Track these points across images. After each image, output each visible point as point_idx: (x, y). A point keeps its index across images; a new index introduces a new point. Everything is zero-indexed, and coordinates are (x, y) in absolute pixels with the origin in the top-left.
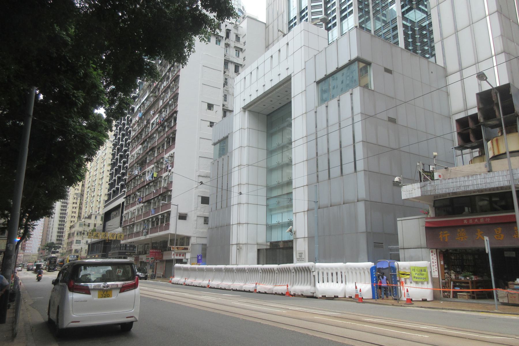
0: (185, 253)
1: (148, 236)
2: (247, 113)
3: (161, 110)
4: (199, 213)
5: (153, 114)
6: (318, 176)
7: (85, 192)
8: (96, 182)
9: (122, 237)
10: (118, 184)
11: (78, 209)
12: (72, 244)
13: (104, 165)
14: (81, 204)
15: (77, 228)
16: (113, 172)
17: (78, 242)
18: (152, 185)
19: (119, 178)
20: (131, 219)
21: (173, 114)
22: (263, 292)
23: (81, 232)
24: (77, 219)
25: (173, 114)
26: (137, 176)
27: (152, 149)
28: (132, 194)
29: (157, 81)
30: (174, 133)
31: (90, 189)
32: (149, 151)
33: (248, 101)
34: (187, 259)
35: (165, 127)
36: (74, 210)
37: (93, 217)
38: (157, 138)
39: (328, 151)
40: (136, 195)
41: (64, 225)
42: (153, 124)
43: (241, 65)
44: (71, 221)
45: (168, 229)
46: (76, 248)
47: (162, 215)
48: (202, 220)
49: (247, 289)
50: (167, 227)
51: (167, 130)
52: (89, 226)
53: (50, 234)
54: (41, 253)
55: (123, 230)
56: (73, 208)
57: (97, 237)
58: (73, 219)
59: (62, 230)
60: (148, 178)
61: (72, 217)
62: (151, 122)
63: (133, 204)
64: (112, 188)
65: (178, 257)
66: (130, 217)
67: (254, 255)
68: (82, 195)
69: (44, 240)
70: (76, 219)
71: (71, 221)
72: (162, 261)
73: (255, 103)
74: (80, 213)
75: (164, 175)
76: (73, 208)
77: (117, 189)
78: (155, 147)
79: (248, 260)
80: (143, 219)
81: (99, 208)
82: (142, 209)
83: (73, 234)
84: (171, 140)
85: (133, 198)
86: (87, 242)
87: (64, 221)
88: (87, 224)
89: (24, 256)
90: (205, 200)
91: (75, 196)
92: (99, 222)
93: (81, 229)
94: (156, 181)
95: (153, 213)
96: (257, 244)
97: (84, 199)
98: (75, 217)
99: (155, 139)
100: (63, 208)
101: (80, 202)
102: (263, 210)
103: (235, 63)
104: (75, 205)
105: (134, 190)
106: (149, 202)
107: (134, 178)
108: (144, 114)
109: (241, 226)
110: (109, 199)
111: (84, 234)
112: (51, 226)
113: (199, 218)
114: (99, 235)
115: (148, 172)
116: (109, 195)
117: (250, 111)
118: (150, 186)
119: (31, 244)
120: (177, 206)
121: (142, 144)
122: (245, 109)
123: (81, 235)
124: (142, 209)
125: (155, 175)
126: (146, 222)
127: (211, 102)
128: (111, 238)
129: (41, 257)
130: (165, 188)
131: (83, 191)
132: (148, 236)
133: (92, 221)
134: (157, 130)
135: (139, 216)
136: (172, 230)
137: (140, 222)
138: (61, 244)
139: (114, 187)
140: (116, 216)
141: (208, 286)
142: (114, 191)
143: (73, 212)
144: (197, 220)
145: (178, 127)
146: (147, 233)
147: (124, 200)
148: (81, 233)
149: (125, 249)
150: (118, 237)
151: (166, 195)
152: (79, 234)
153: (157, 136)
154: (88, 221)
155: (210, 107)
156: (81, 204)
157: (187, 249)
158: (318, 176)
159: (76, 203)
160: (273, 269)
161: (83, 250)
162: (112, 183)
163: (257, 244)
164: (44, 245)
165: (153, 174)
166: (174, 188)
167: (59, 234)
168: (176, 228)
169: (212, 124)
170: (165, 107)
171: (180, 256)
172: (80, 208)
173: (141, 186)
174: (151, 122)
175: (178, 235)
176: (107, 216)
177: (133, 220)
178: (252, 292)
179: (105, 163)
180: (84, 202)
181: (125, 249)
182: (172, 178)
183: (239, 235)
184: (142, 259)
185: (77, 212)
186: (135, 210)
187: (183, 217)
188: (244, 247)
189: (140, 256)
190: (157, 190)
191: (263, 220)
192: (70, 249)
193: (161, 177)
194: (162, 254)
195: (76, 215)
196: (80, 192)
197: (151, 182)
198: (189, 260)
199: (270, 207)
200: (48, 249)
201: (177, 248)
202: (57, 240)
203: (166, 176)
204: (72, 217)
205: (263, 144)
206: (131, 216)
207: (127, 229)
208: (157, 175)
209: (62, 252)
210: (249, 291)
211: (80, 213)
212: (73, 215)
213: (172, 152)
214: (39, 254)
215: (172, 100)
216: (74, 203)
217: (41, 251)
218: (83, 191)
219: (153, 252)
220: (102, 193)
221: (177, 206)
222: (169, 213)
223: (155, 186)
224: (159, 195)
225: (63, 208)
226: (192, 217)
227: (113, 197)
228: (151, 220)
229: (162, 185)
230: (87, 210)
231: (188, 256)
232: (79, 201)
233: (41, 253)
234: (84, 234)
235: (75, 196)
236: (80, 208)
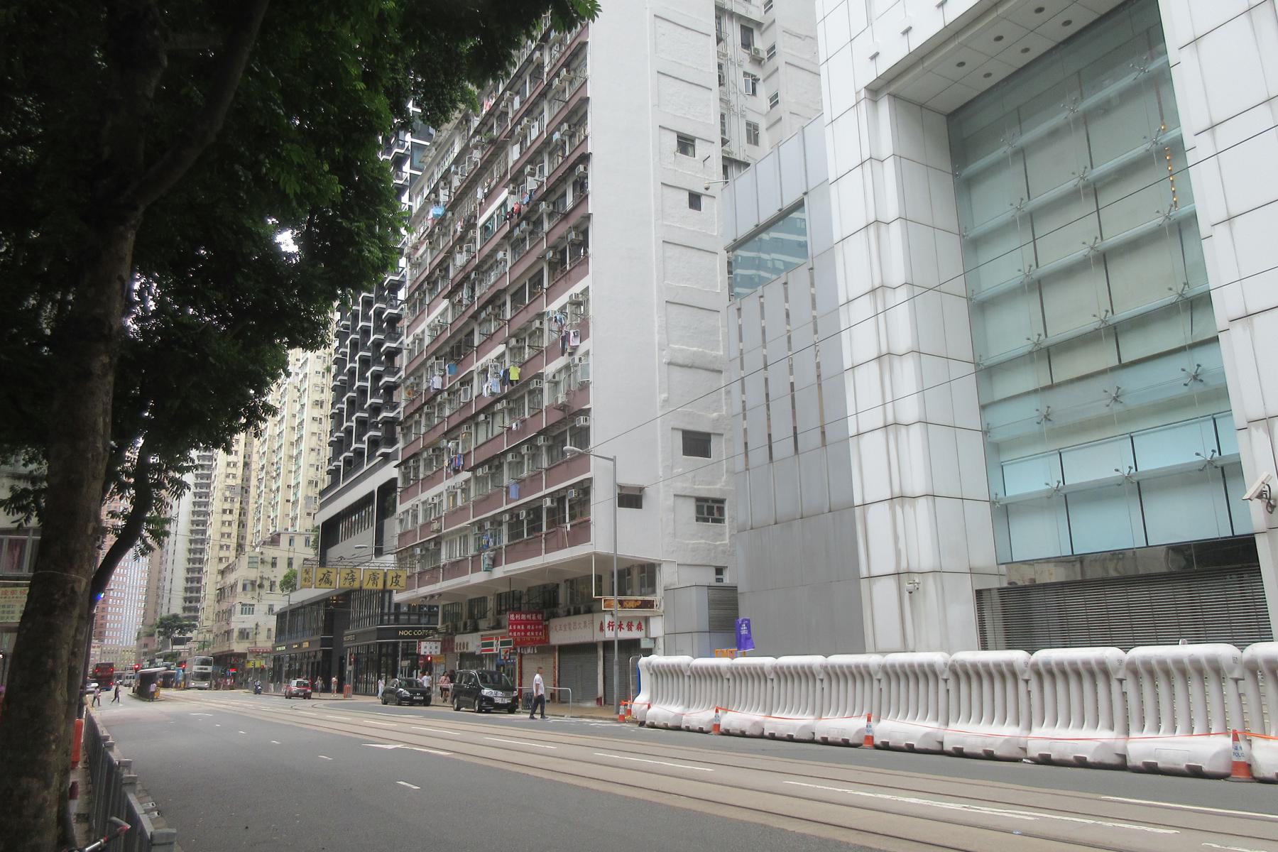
0: (647, 619)
1: (499, 572)
2: (885, 107)
3: (521, 171)
4: (682, 486)
5: (486, 196)
6: (823, 433)
7: (254, 482)
8: (282, 454)
9: (402, 581)
10: (359, 440)
11: (235, 526)
12: (230, 616)
13: (303, 406)
14: (243, 512)
15: (244, 572)
16: (341, 410)
17: (248, 609)
18: (502, 411)
19: (362, 423)
20: (427, 525)
21: (572, 168)
22: (980, 751)
23: (253, 583)
24: (234, 553)
25: (572, 168)
26: (439, 392)
27: (495, 300)
28: (425, 448)
29: (530, 37)
30: (583, 232)
31: (267, 473)
32: (483, 308)
33: (895, 52)
34: (655, 639)
35: (538, 223)
36: (226, 530)
37: (284, 540)
38: (509, 264)
39: (744, 409)
40: (438, 451)
41: (200, 570)
42: (485, 228)
43: (759, 25)
44: (221, 559)
45: (587, 539)
46: (243, 626)
47: (559, 498)
48: (690, 509)
49: (695, 724)
50: (582, 532)
51: (546, 227)
52: (274, 564)
53: (166, 595)
54: (146, 645)
55: (400, 560)
56: (223, 523)
57: (328, 582)
58: (223, 554)
59: (195, 585)
60: (491, 386)
61: (221, 547)
62: (481, 222)
63: (430, 481)
64: (341, 453)
65: (625, 634)
66: (420, 520)
67: (964, 612)
68: (245, 490)
69: (151, 612)
70: (232, 554)
71: (221, 559)
72: (544, 648)
73: (958, 33)
74: (241, 537)
75: (550, 369)
76: (223, 523)
77: (359, 453)
78: (504, 290)
79: (949, 637)
80: (472, 520)
81: (294, 519)
82: (465, 491)
83: (233, 587)
84: (570, 254)
85: (429, 463)
86: (271, 609)
87: (201, 561)
88: (270, 560)
89: (103, 653)
90: (697, 444)
91: (228, 494)
92: (304, 552)
93: (253, 574)
94: (517, 393)
95: (513, 494)
96: (972, 572)
97: (251, 501)
98: (228, 547)
99: (500, 267)
100: (195, 527)
101: (242, 509)
102: (974, 446)
103: (740, 17)
104: (227, 517)
105: (433, 436)
106: (494, 463)
107: (431, 401)
108: (452, 207)
109: (907, 507)
110: (335, 483)
111: (261, 586)
112: (168, 575)
113: (680, 501)
114: (332, 577)
115: (485, 371)
116: (334, 473)
117: (894, 97)
118: (494, 414)
119: (118, 622)
120: (613, 460)
121: (449, 296)
122: (874, 91)
123: (253, 589)
124: (465, 491)
125: (514, 375)
126: (488, 525)
127: (688, 130)
128: (370, 586)
129: (145, 654)
130: (563, 408)
131: (246, 479)
132: (499, 572)
133: (281, 552)
134: (507, 236)
135: (456, 513)
136: (599, 542)
137: (461, 529)
138: (196, 618)
139: (348, 449)
140: (361, 524)
141: (717, 726)
142: (348, 462)
143: (223, 535)
144: (674, 510)
145: (593, 206)
146: (495, 562)
147: (395, 473)
148: (255, 585)
149: (397, 620)
150: (389, 583)
151: (569, 429)
152: (249, 587)
153: (509, 257)
154: (271, 552)
155: (686, 144)
156: (243, 512)
157: (648, 605)
158: (823, 433)
159: (231, 512)
160: (762, 668)
161: (260, 629)
162: (340, 440)
163: (972, 572)
164: (151, 622)
165: (507, 372)
166: (595, 401)
167: (188, 595)
168: (610, 534)
169: (695, 200)
170: (534, 159)
171: (630, 627)
172: (242, 525)
173: (456, 420)
174: (481, 222)
175: (620, 559)
176: (329, 533)
177: (435, 526)
178: (707, 732)
179: (305, 400)
180: (252, 507)
181: (397, 620)
182: (586, 371)
183: (883, 542)
184: (466, 645)
185: (234, 534)
186: (440, 495)
187: (630, 499)
188: (930, 584)
189: (458, 639)
190: (524, 421)
191: (977, 485)
192: (226, 628)
193: (540, 376)
194: (546, 628)
195: (233, 542)
196: (239, 481)
197: (498, 400)
198: (661, 642)
199: (997, 436)
200: (164, 634)
201: (621, 602)
202: (185, 609)
203: (560, 371)
204: (221, 547)
205: (946, 215)
206: (425, 517)
207: (413, 556)
208: (520, 375)
209: (201, 637)
210: (846, 744)
211: (241, 537)
212: (225, 541)
213: (577, 288)
214: (139, 647)
215: (566, 126)
216: (224, 511)
217: (143, 641)
218: (246, 479)
219: (516, 622)
220: (300, 479)
221: (613, 460)
222: (584, 489)
223: (511, 411)
224: (539, 433)
225: (195, 527)
226: (659, 499)
227: (346, 476)
228: (507, 517)
229: (546, 403)
230: (260, 527)
231: (657, 628)
232: (237, 505)
233: (146, 645)
234: (261, 586)
235: (228, 494)
236: (242, 525)
